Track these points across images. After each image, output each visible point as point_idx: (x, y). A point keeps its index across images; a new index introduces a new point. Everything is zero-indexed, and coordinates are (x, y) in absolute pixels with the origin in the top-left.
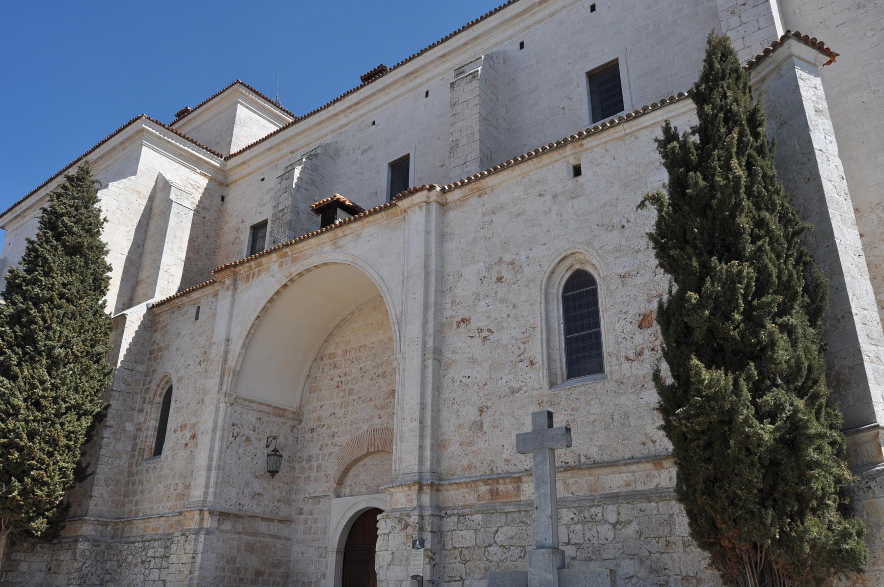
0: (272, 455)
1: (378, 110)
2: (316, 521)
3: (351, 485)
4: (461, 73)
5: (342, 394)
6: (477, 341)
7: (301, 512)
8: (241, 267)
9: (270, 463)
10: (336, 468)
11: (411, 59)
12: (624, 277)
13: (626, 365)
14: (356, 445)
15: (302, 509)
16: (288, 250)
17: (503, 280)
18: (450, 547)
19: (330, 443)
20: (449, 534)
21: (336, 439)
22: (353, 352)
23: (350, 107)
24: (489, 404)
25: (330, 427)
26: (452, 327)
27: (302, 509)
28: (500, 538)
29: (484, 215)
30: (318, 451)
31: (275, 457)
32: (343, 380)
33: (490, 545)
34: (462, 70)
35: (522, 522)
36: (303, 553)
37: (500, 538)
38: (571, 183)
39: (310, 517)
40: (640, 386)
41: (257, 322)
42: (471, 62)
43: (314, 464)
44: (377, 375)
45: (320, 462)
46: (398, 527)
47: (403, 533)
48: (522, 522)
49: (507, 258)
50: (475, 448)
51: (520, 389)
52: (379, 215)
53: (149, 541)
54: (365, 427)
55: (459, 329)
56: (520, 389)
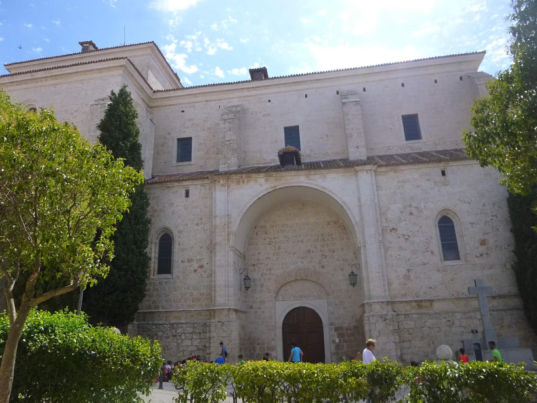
2: (263, 312)
3: (282, 295)
4: (346, 98)
5: (273, 248)
6: (402, 240)
7: (251, 307)
8: (234, 176)
12: (472, 223)
13: (476, 259)
15: (252, 306)
18: (402, 328)
19: (268, 273)
20: (401, 322)
21: (272, 272)
23: (253, 88)
24: (412, 268)
27: (252, 306)
28: (427, 324)
29: (398, 182)
30: (260, 277)
32: (273, 241)
33: (423, 327)
34: (347, 96)
35: (438, 318)
36: (256, 329)
37: (427, 324)
38: (442, 178)
40: (185, 223)
45: (262, 282)
46: (381, 320)
47: (384, 323)
48: (438, 318)
49: (414, 204)
50: (407, 286)
51: (428, 263)
53: (177, 324)
55: (392, 233)
56: (428, 263)
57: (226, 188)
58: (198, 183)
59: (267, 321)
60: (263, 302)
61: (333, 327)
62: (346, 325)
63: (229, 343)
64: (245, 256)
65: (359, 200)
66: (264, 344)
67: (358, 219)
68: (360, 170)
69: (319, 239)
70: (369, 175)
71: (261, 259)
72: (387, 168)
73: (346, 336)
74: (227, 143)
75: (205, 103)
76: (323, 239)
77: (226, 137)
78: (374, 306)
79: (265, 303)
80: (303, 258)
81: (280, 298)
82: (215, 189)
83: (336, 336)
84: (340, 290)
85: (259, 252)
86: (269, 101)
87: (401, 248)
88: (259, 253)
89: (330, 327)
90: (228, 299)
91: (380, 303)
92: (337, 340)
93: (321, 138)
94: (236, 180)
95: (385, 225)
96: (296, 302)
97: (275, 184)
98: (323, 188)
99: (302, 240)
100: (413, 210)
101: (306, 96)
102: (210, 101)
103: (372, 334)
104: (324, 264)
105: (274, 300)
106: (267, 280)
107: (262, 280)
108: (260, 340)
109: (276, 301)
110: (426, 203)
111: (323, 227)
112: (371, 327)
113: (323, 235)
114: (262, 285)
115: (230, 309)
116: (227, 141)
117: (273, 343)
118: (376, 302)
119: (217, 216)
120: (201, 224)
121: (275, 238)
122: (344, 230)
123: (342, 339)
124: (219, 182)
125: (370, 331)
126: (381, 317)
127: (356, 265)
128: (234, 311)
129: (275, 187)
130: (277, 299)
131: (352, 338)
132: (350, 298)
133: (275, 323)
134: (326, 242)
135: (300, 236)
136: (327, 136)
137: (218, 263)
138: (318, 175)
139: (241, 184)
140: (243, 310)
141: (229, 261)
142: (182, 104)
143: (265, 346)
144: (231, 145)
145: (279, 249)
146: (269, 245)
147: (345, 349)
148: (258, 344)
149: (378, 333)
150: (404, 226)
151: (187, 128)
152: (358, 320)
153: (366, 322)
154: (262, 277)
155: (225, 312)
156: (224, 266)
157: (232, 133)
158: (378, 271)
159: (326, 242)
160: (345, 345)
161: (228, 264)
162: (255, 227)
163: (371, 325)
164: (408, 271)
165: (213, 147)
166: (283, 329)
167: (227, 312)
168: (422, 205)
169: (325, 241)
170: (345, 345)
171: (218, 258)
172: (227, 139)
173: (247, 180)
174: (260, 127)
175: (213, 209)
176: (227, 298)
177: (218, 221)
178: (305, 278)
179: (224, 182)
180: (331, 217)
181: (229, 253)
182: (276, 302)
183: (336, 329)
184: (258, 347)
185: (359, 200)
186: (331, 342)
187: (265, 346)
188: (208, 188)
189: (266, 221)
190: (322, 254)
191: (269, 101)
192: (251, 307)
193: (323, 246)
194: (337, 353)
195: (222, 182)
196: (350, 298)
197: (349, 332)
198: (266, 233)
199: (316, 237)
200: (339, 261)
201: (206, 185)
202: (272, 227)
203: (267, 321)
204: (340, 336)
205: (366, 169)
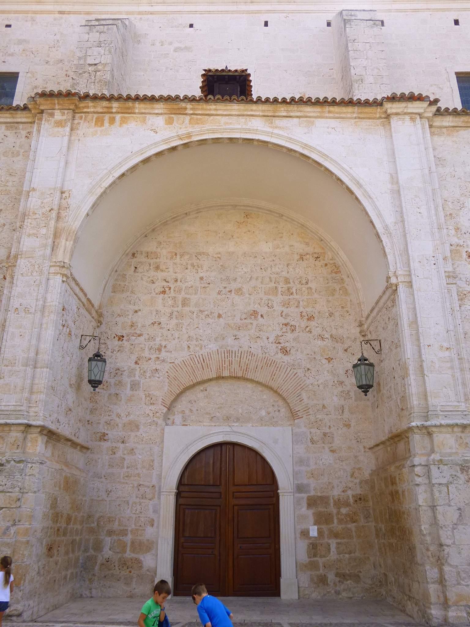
0: (359, 365)
1: (197, 15)
2: (132, 451)
3: (183, 411)
5: (170, 302)
7: (103, 437)
8: (91, 104)
10: (166, 388)
14: (199, 366)
15: (104, 435)
16: (189, 106)
19: (153, 357)
21: (163, 354)
25: (153, 338)
26: (461, 257)
27: (104, 435)
30: (133, 365)
31: (363, 367)
36: (108, 492)
39: (122, 445)
41: (323, 169)
42: (364, 10)
43: (127, 380)
44: (228, 289)
52: (350, 109)
54: (213, 347)
57: (68, 129)
59: (138, 475)
60: (134, 426)
61: (305, 496)
62: (336, 492)
63: (8, 528)
64: (100, 315)
65: (394, 179)
66: (124, 533)
67: (390, 219)
68: (397, 114)
69: (280, 290)
70: (419, 126)
72: (457, 119)
73: (335, 521)
74: (91, 69)
75: (57, 16)
77: (88, 58)
78: (439, 437)
79: (138, 427)
81: (178, 418)
82: (39, 131)
83: (311, 519)
85: (137, 308)
86: (191, 26)
88: (136, 312)
89: (297, 495)
90: (29, 400)
91: (456, 429)
92: (314, 532)
94: (96, 116)
95: (455, 240)
96: (217, 429)
97: (190, 130)
98: (306, 146)
99: (240, 289)
101: (266, 24)
102: (69, 13)
103: (440, 517)
104: (287, 344)
105: (160, 421)
106: (148, 375)
107: (137, 373)
108: (117, 523)
109: (167, 425)
112: (437, 494)
113: (287, 281)
114: (135, 386)
115: (29, 426)
116: (90, 65)
117: (150, 532)
118: (448, 426)
119: (34, 189)
122: (336, 273)
123: (324, 527)
124: (52, 115)
125: (433, 508)
127: (372, 342)
128: (41, 432)
129: (189, 135)
130: (169, 422)
131: (352, 526)
132: (348, 426)
133: (160, 477)
135: (235, 280)
137: (15, 303)
138: (296, 120)
139: (106, 124)
140: (79, 441)
141: (49, 300)
142: (9, 12)
143: (129, 538)
144: (98, 73)
145: (184, 304)
146: (162, 295)
147: (333, 555)
148: (110, 533)
149: (457, 515)
151: (12, 55)
152: (366, 482)
153: (418, 480)
154: (137, 366)
155: (15, 435)
156: (33, 310)
158: (446, 345)
159: (295, 296)
160: (333, 543)
161: (44, 307)
162: (133, 255)
163: (435, 490)
166: (178, 495)
167: (19, 435)
170: (333, 543)
171: (18, 289)
172: (90, 61)
173: (122, 118)
174: (167, 68)
175: (28, 175)
176: (26, 395)
177: (34, 202)
178: (240, 375)
179: (65, 117)
180: (307, 244)
181: (51, 282)
182: (167, 429)
183: (312, 502)
184: (108, 540)
185: (394, 179)
186: (298, 535)
187: (129, 538)
188: (24, 133)
190: (285, 322)
191: (191, 26)
192: (103, 437)
193: (286, 304)
194: (313, 566)
195: (58, 115)
196: (348, 426)
197: (344, 511)
198: (157, 268)
199: (273, 285)
201: (21, 126)
202: (172, 258)
203: (138, 475)
205: (410, 111)
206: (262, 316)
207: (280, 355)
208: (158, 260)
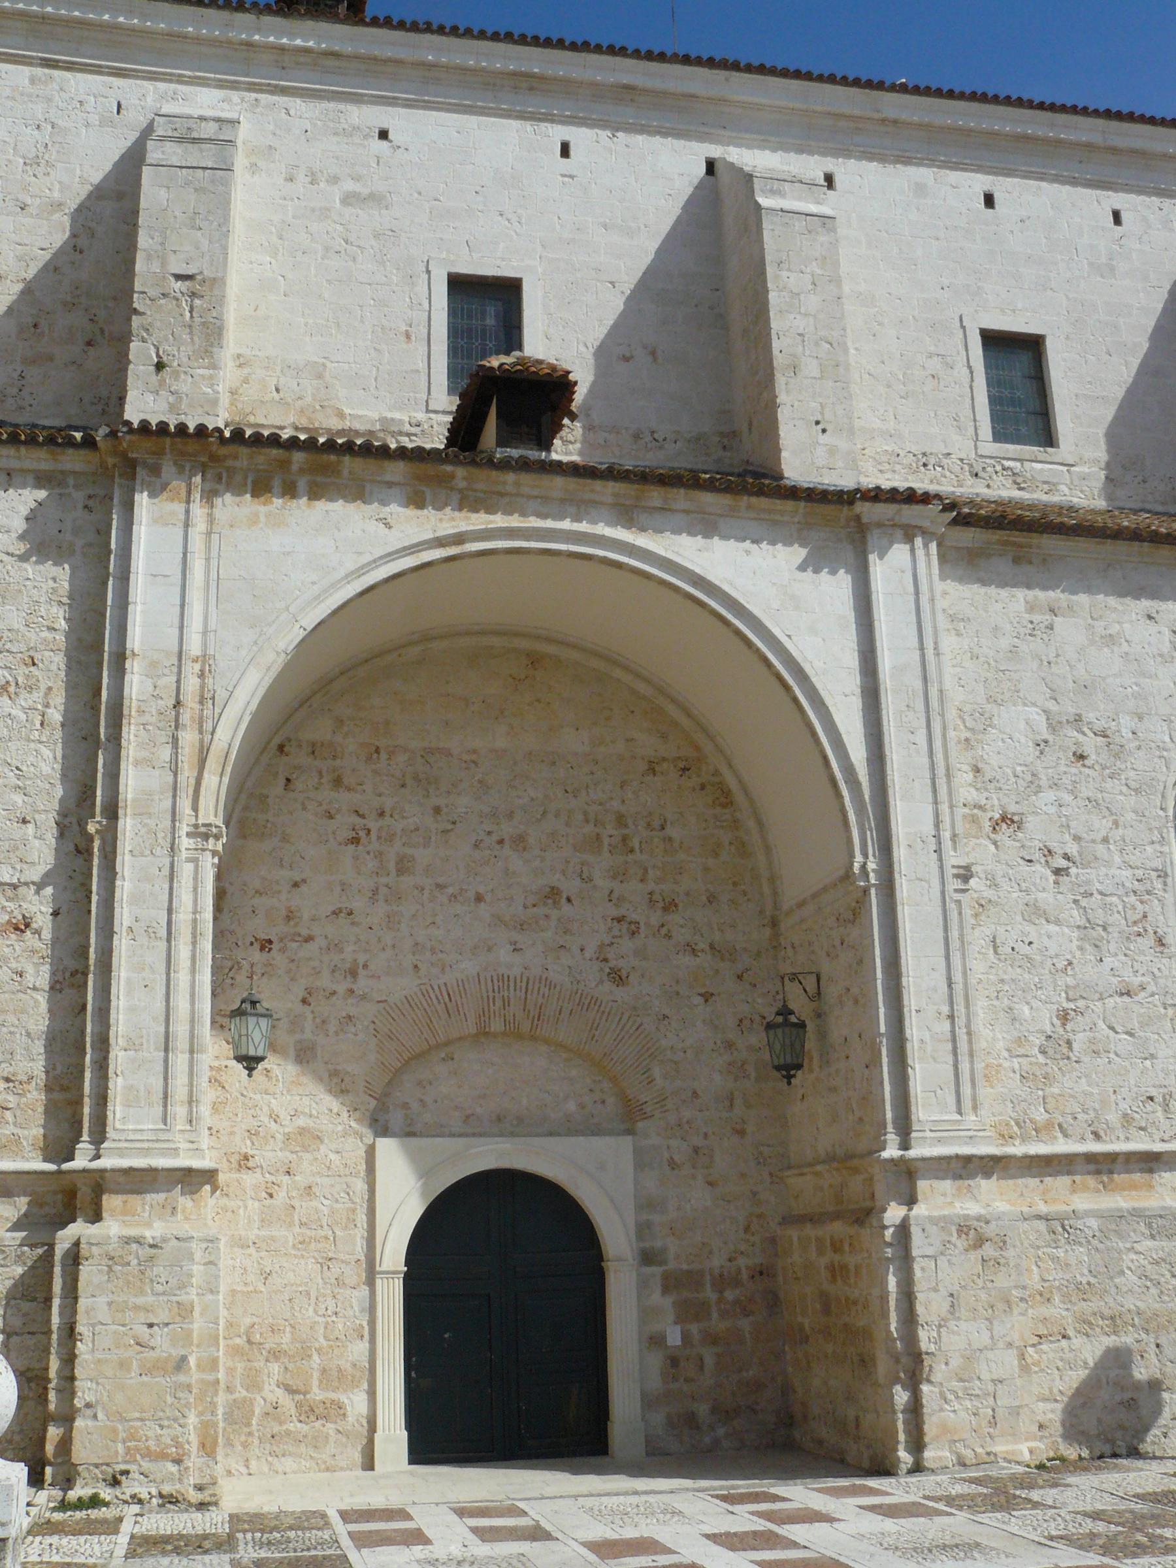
0: (778, 1026)
3: (405, 1106)
5: (371, 864)
6: (1041, 870)
9: (778, 1047)
11: (548, 43)
14: (440, 1008)
17: (1086, 762)
19: (341, 988)
21: (363, 984)
22: (402, 758)
31: (787, 1030)
32: (374, 826)
45: (308, 1035)
46: (961, 1243)
47: (975, 1256)
54: (468, 967)
58: (27, 464)
62: (717, 1262)
68: (880, 525)
69: (606, 841)
71: (306, 916)
73: (715, 1315)
76: (625, 839)
77: (172, 258)
80: (522, 926)
84: (695, 1094)
87: (1035, 912)
88: (296, 885)
92: (674, 1337)
93: (626, 359)
100: (1090, 744)
104: (621, 963)
106: (332, 1027)
110: (1141, 719)
111: (623, 785)
120: (30, 689)
121: (382, 814)
122: (723, 806)
123: (694, 1328)
126: (963, 1230)
132: (741, 1133)
134: (637, 856)
136: (653, 353)
145: (401, 871)
149: (946, 1305)
150: (1052, 810)
157: (205, 244)
164: (1064, 1017)
165: (69, 306)
168: (1126, 723)
169: (632, 851)
183: (670, 1283)
189: (340, 722)
190: (615, 912)
193: (619, 875)
196: (741, 1133)
197: (730, 1295)
198: (338, 782)
199: (589, 829)
200: (694, 952)
202: (369, 759)
204: (689, 1312)
206: (569, 900)
207: (608, 986)
208: (338, 762)
